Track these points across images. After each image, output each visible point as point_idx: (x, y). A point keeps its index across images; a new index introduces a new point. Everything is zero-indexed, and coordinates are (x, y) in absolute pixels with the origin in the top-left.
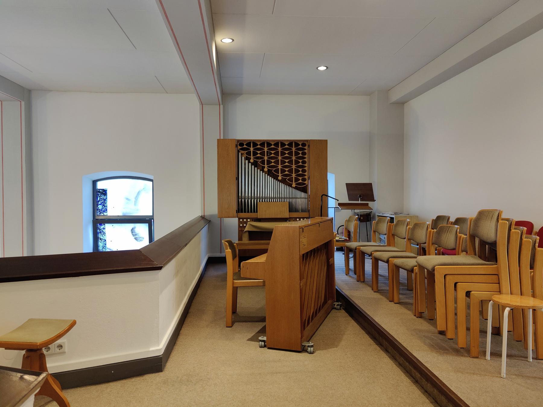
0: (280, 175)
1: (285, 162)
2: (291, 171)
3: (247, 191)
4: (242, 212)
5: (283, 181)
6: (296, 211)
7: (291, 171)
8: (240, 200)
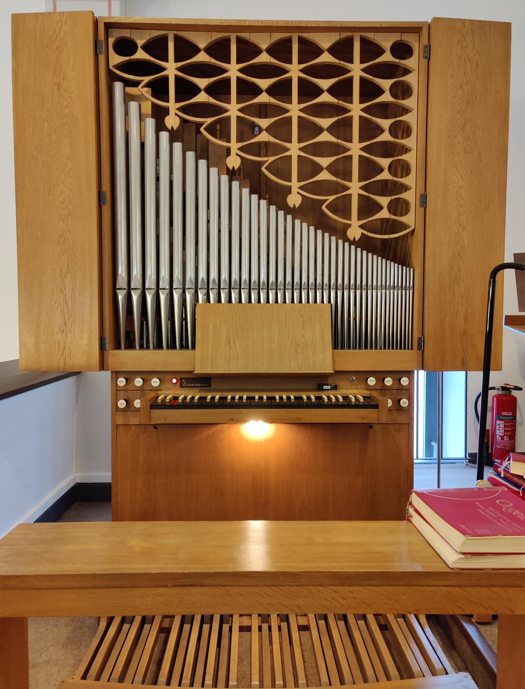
0: (295, 184)
1: (319, 130)
2: (342, 169)
3: (144, 270)
5: (309, 213)
6: (365, 342)
7: (281, 130)
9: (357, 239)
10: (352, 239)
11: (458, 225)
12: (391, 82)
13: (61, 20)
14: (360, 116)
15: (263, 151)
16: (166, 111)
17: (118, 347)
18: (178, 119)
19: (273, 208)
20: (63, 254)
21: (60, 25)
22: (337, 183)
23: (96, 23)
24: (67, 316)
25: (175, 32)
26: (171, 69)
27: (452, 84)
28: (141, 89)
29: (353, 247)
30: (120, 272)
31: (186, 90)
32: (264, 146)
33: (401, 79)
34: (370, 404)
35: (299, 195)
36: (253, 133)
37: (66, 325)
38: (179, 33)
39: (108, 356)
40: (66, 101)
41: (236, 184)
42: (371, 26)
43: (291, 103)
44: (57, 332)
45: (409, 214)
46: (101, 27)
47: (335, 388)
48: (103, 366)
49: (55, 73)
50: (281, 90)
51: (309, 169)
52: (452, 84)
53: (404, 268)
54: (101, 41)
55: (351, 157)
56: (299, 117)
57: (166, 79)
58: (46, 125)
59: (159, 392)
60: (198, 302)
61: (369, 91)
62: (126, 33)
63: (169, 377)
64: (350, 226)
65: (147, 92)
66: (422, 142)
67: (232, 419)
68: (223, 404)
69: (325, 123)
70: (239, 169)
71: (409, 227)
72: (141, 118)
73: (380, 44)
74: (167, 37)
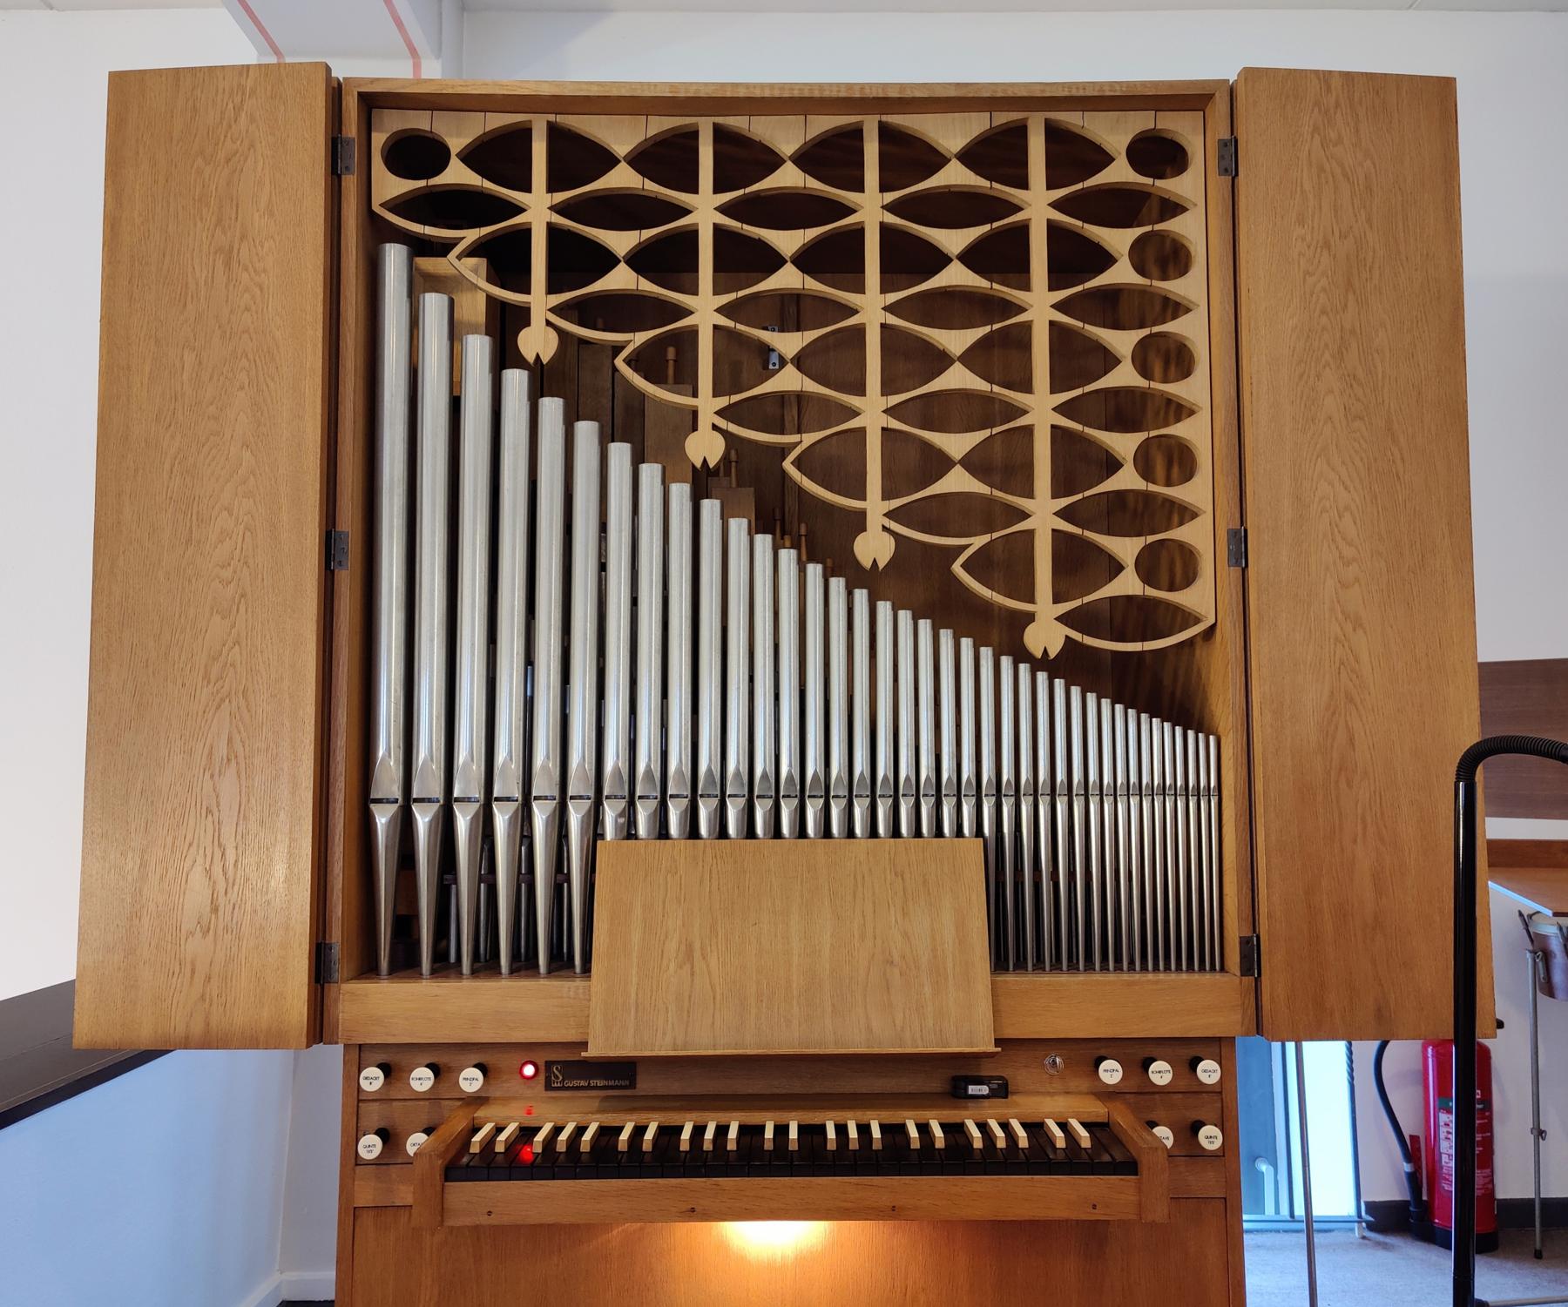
0: (875, 506)
1: (940, 361)
2: (1005, 464)
3: (475, 727)
4: (405, 964)
5: (922, 585)
8: (383, 818)
9: (1052, 655)
10: (1039, 654)
11: (1340, 616)
12: (1133, 234)
13: (239, 85)
14: (1052, 323)
15: (791, 414)
16: (522, 316)
17: (368, 969)
18: (553, 338)
19: (814, 571)
20: (219, 707)
21: (238, 99)
22: (989, 500)
23: (336, 92)
24: (221, 886)
25: (552, 117)
26: (538, 208)
27: (1303, 239)
28: (456, 263)
29: (1042, 677)
30: (381, 751)
31: (575, 260)
32: (794, 400)
33: (1158, 227)
34: (1107, 1154)
35: (886, 534)
36: (766, 367)
37: (215, 910)
38: (560, 119)
39: (337, 1000)
40: (247, 295)
41: (710, 508)
42: (1074, 93)
43: (860, 289)
44: (192, 934)
45: (1198, 584)
46: (351, 106)
47: (1002, 1091)
48: (319, 1028)
49: (219, 221)
50: (836, 258)
51: (913, 465)
52: (1303, 239)
53: (1191, 734)
54: (349, 141)
55: (1028, 431)
56: (883, 326)
57: (525, 233)
58: (189, 358)
59: (481, 1113)
60: (602, 836)
61: (1074, 258)
62: (420, 121)
63: (512, 1059)
64: (1030, 618)
65: (475, 271)
66: (1224, 392)
67: (693, 1210)
68: (668, 1160)
69: (956, 341)
70: (726, 458)
71: (1197, 621)
72: (454, 333)
73: (1098, 140)
74: (530, 130)
